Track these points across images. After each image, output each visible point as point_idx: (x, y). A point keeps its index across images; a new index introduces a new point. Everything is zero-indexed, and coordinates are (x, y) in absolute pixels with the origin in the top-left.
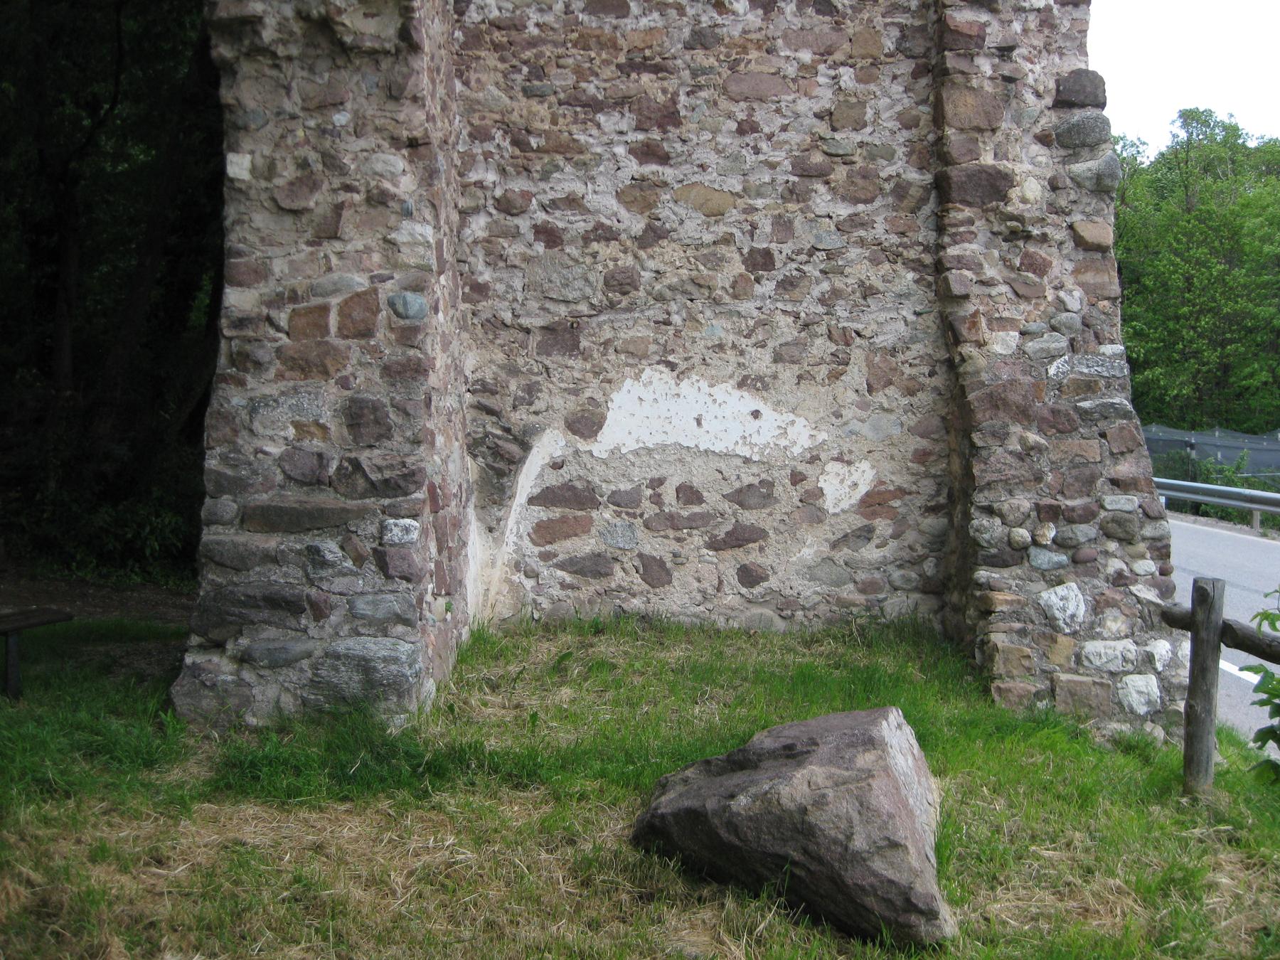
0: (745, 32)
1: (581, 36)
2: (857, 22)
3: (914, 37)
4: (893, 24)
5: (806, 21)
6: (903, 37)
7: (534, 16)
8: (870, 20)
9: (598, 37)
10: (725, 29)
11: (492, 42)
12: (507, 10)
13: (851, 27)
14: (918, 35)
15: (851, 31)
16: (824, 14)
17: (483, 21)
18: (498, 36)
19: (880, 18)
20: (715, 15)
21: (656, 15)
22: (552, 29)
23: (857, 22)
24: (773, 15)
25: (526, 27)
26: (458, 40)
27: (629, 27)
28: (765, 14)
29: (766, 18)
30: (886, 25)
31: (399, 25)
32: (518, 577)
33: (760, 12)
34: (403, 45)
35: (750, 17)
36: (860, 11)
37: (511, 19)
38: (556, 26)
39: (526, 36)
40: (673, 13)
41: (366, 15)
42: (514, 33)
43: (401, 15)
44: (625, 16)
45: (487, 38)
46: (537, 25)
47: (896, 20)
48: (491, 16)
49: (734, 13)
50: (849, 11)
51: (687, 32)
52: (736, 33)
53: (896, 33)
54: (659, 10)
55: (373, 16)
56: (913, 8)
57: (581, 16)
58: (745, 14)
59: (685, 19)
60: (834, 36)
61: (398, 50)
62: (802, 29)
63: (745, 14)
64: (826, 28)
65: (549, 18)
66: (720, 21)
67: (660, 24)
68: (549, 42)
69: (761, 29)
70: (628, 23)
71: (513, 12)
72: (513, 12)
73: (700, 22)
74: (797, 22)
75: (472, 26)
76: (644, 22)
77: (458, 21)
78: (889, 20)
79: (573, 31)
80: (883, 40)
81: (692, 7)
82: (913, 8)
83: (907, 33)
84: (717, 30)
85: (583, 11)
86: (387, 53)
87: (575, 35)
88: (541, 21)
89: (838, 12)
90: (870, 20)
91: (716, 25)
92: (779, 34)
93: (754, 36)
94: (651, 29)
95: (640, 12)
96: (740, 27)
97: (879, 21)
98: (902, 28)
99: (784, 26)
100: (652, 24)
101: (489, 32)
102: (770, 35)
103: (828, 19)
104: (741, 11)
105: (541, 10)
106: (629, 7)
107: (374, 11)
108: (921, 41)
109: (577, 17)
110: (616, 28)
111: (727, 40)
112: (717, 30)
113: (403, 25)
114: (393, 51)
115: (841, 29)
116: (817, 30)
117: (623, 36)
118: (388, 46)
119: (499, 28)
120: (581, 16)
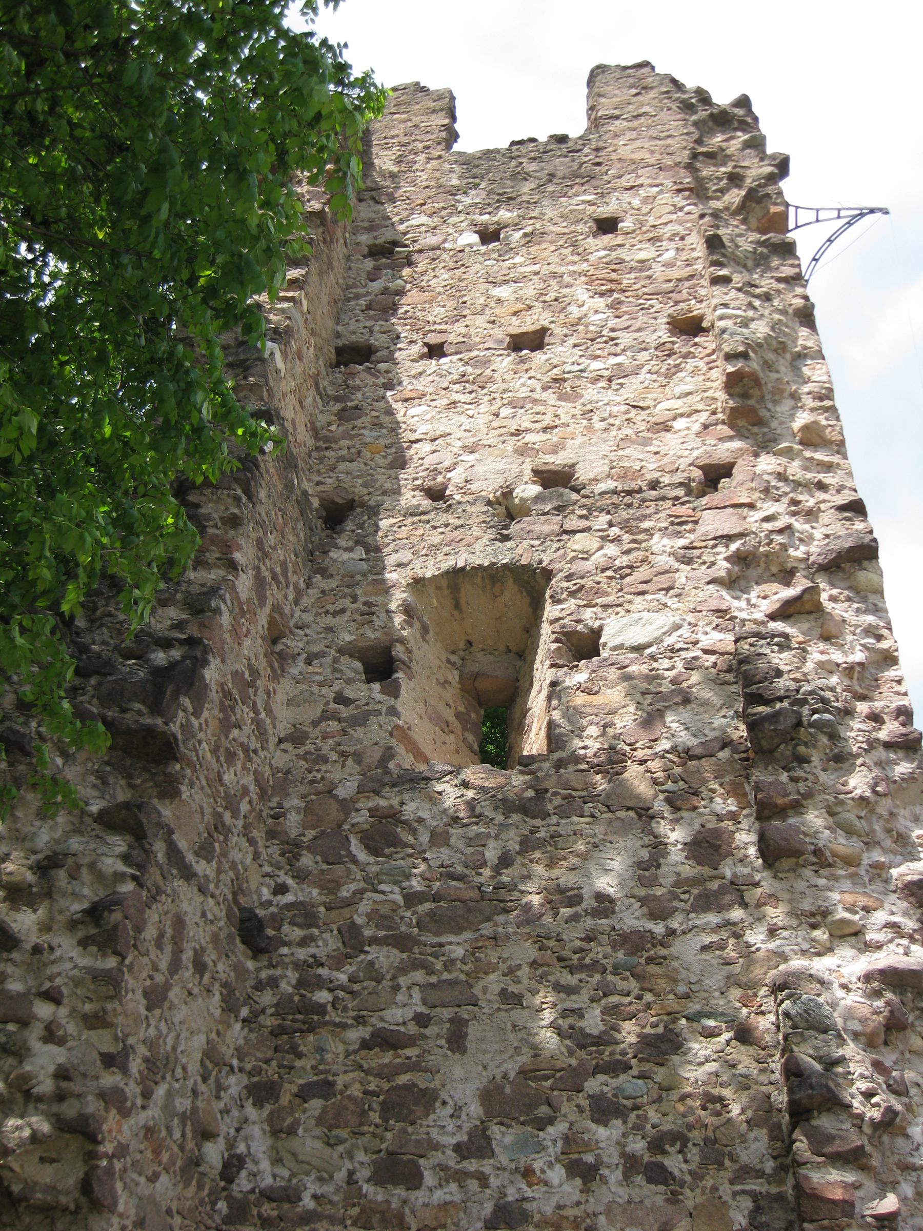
0: (560, 1207)
1: (363, 1211)
2: (698, 1191)
3: (771, 1208)
4: (744, 1192)
5: (636, 1194)
6: (757, 1210)
7: (312, 1187)
8: (715, 1189)
9: (383, 1213)
10: (535, 1204)
11: (260, 1215)
12: (283, 1178)
13: (691, 1199)
14: (775, 1205)
15: (690, 1204)
16: (657, 1183)
17: (252, 1191)
18: (268, 1209)
19: (727, 1185)
20: (524, 1187)
21: (453, 1187)
22: (331, 1202)
23: (698, 1191)
24: (594, 1186)
25: (300, 1199)
26: (220, 1211)
27: (420, 1201)
28: (585, 1183)
29: (585, 1190)
30: (735, 1194)
31: (81, 1175)
32: (797, 262)
33: (578, 1182)
34: (83, 1200)
35: (567, 1188)
36: (702, 1178)
37: (285, 1189)
38: (335, 1198)
39: (299, 1209)
40: (473, 1185)
41: (42, 1160)
42: (286, 1206)
43: (85, 1162)
44: (417, 1187)
45: (255, 1211)
46: (315, 1197)
47: (747, 1187)
48: (263, 1185)
49: (546, 1184)
50: (688, 1178)
51: (488, 1208)
52: (549, 1209)
53: (747, 1203)
54: (458, 1180)
55: (53, 1161)
56: (768, 1170)
57: (365, 1187)
58: (561, 1185)
59: (488, 1191)
60: (670, 1209)
61: (78, 1208)
62: (629, 1202)
63: (561, 1185)
64: (659, 1200)
65: (328, 1189)
66: (529, 1193)
67: (457, 1198)
68: (326, 1217)
69: (578, 1203)
70: (419, 1197)
71: (290, 1180)
72: (290, 1180)
73: (505, 1195)
74: (623, 1194)
75: (239, 1196)
76: (439, 1196)
77: (224, 1189)
78: (738, 1188)
79: (354, 1205)
80: (732, 1213)
81: (497, 1176)
82: (768, 1170)
83: (762, 1203)
84: (526, 1205)
85: (368, 1181)
86: (65, 1209)
87: (355, 1211)
88: (319, 1192)
89: (674, 1179)
90: (715, 1189)
91: (525, 1199)
92: (601, 1209)
93: (570, 1212)
94: (446, 1203)
95: (436, 1183)
96: (554, 1201)
97: (726, 1190)
98: (755, 1196)
99: (607, 1197)
100: (448, 1198)
101: (258, 1205)
102: (590, 1211)
103: (661, 1188)
104: (556, 1181)
105: (320, 1179)
106: (421, 1176)
107: (54, 1155)
108: (780, 1213)
109: (361, 1188)
110: (405, 1202)
111: (537, 1218)
112: (526, 1205)
113: (86, 1174)
114: (72, 1207)
115: (678, 1201)
116: (647, 1203)
117: (413, 1212)
118: (63, 1200)
119: (270, 1199)
120: (365, 1187)
